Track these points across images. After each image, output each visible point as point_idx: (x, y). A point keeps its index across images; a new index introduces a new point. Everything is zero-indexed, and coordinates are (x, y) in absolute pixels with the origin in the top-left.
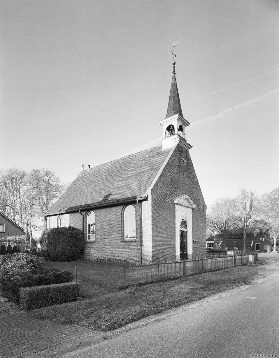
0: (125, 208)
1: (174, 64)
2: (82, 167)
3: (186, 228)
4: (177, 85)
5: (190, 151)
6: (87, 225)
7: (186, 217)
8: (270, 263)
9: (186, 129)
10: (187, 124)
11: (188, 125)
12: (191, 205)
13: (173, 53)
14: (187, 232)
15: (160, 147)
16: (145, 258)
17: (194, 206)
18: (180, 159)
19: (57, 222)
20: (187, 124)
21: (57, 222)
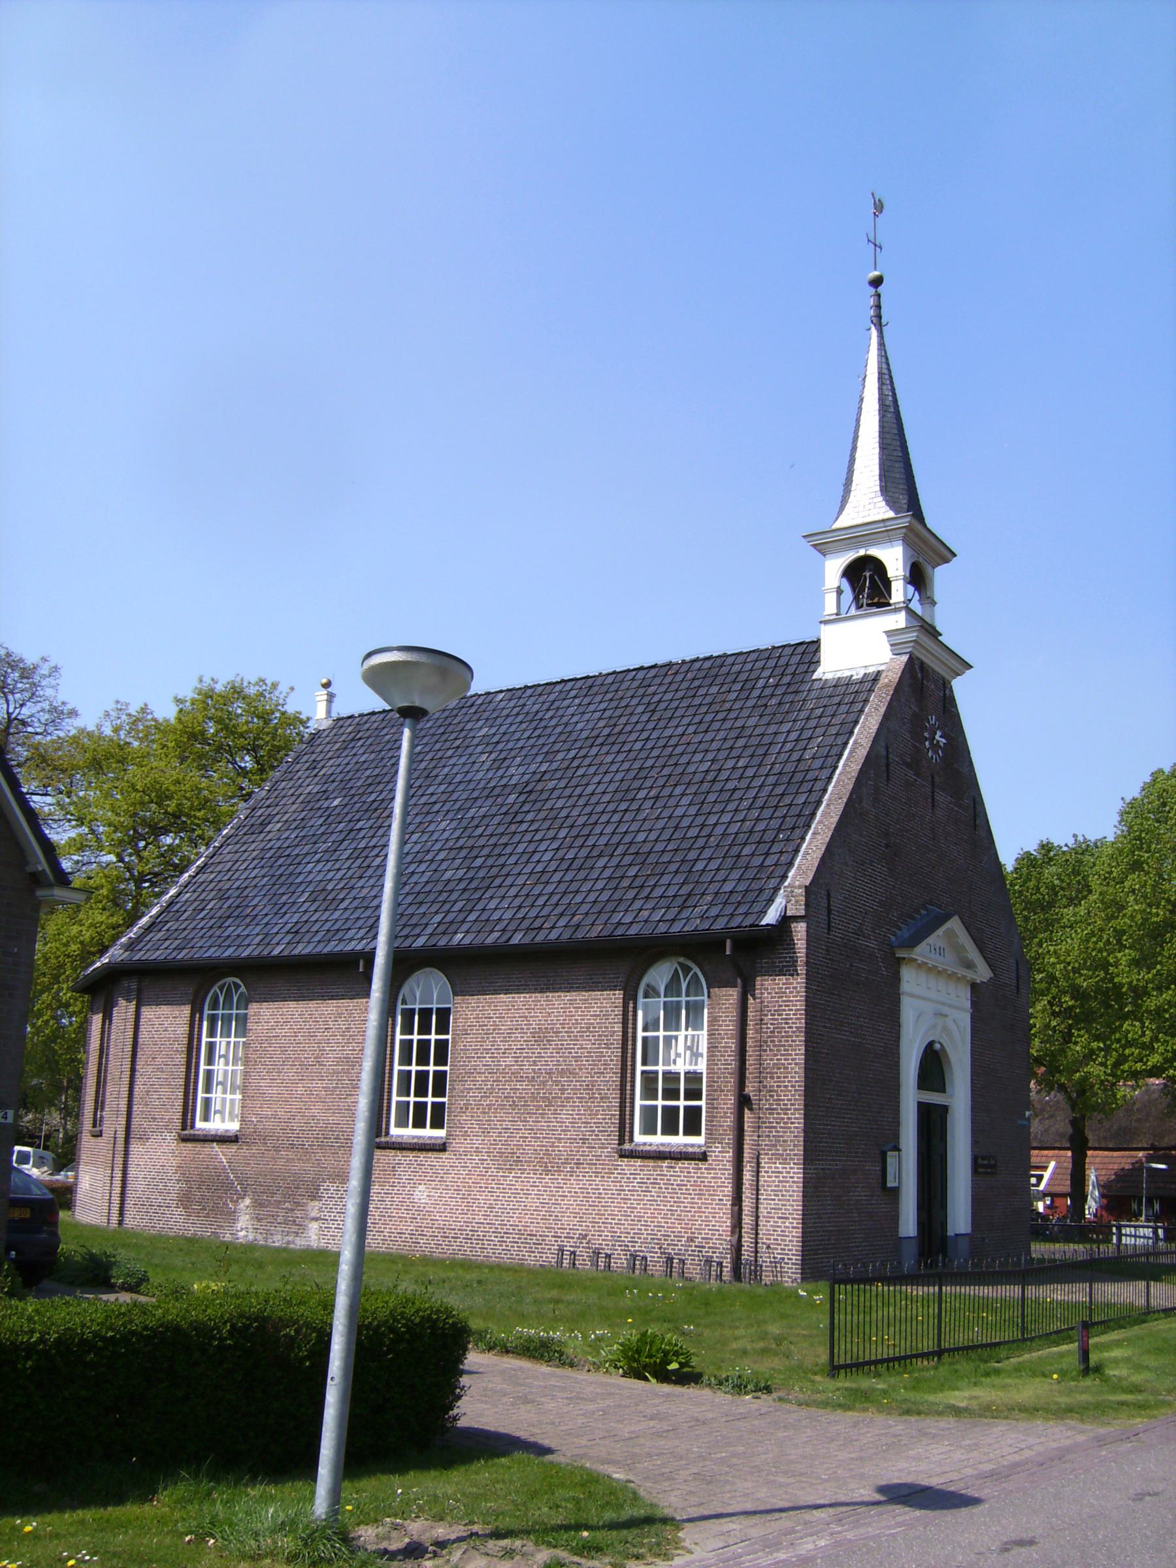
0: (1030, 1411)
1: (877, 282)
2: (322, 695)
3: (942, 1089)
4: (893, 374)
5: (960, 687)
6: (389, 1103)
7: (945, 1029)
8: (47, 1187)
9: (941, 576)
10: (945, 554)
11: (947, 561)
12: (969, 965)
13: (872, 239)
14: (944, 1110)
15: (810, 651)
16: (765, 1258)
17: (983, 973)
18: (917, 725)
19: (737, 1199)
20: (945, 554)
21: (737, 1199)
